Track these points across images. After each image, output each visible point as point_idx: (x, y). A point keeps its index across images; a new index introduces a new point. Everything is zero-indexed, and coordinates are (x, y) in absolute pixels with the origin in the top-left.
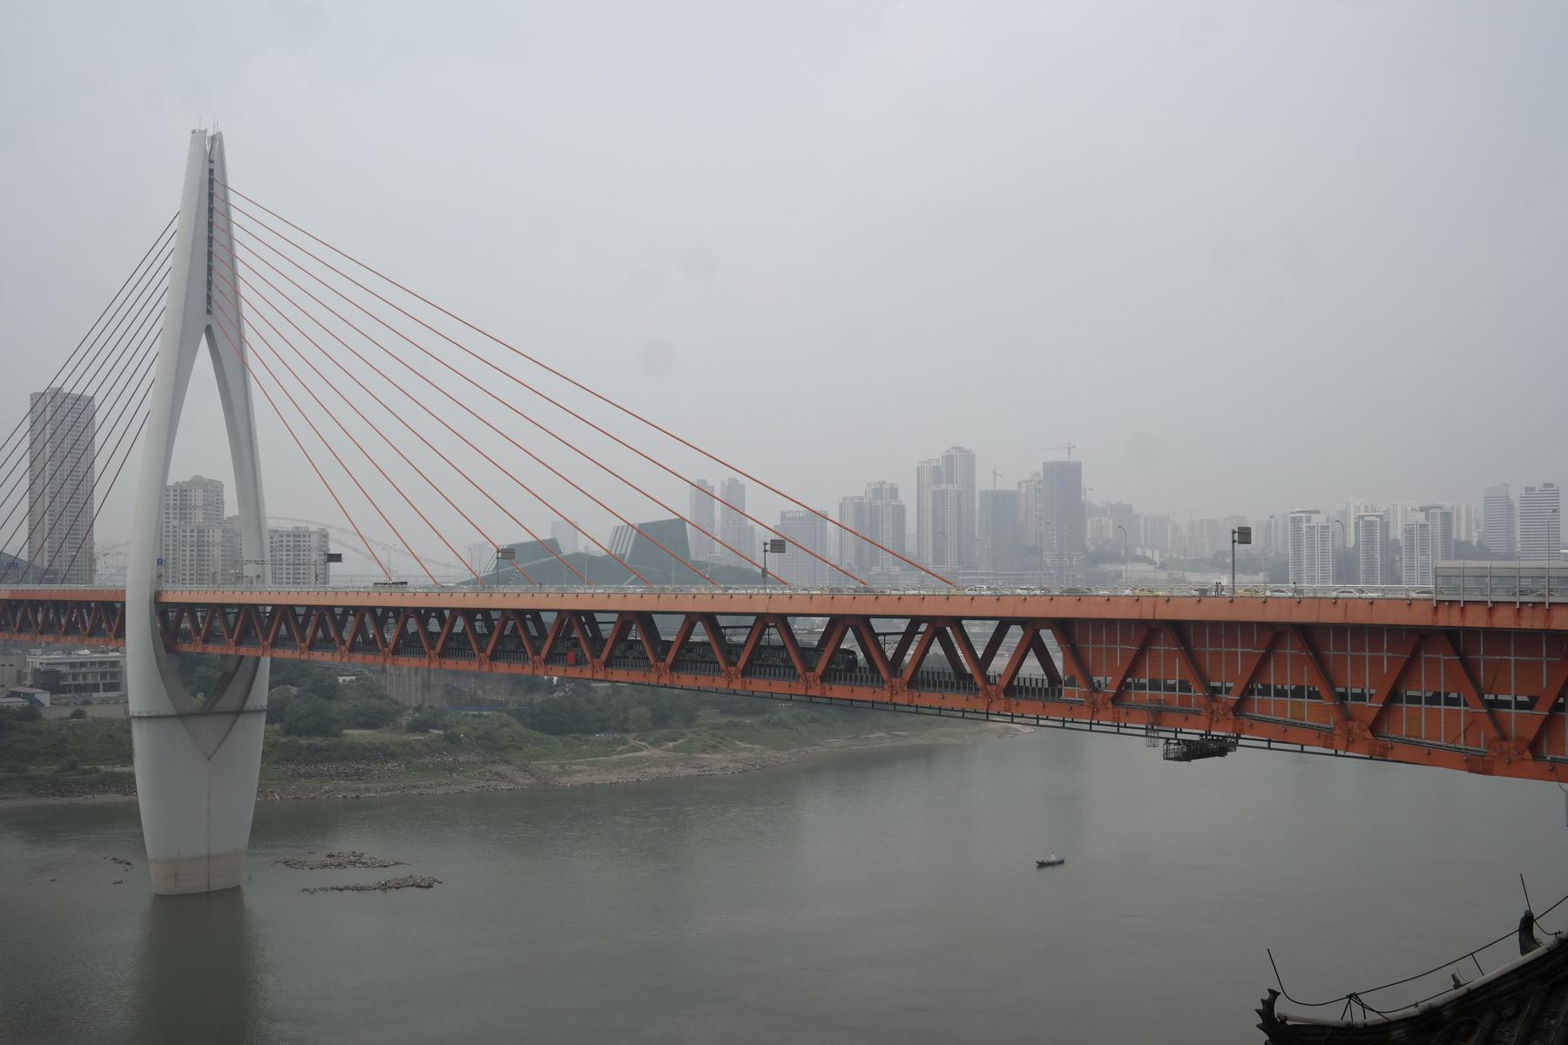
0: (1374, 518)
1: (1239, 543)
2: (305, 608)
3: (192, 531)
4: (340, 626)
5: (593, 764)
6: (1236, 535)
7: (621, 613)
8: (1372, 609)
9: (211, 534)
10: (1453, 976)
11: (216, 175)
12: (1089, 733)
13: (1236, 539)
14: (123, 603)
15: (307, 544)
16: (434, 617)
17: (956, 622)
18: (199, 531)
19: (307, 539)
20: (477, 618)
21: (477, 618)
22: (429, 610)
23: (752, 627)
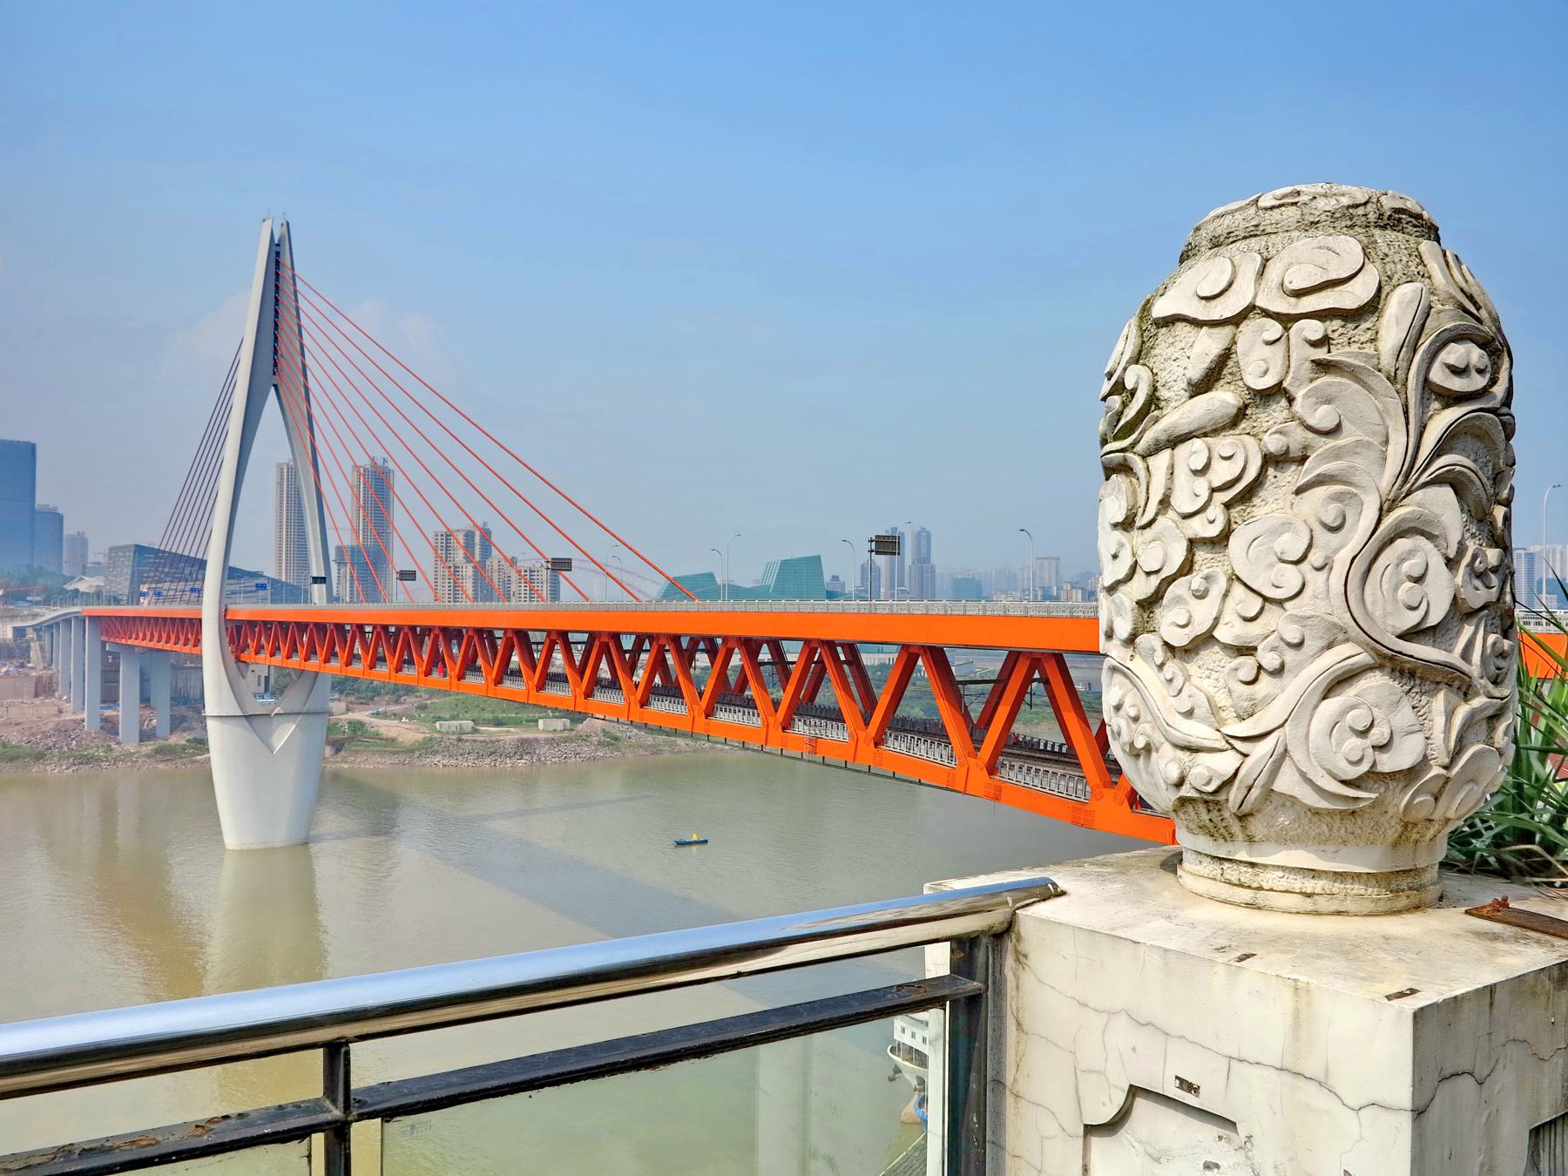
0: (1478, 482)
1: (877, 553)
2: (634, 637)
3: (526, 571)
4: (686, 658)
5: (1498, 912)
6: (874, 543)
7: (549, 632)
8: (1162, 638)
9: (464, 569)
10: (1177, 1078)
11: (286, 259)
12: (843, 771)
13: (873, 547)
14: (200, 620)
15: (540, 577)
16: (702, 651)
17: (1058, 658)
18: (531, 571)
19: (540, 574)
20: (700, 648)
21: (700, 648)
22: (694, 641)
23: (372, 633)
